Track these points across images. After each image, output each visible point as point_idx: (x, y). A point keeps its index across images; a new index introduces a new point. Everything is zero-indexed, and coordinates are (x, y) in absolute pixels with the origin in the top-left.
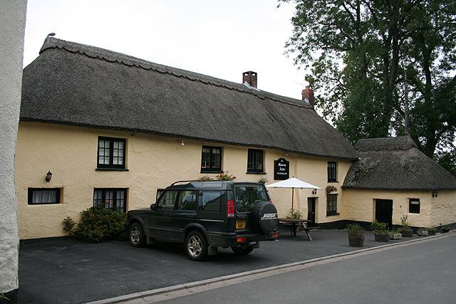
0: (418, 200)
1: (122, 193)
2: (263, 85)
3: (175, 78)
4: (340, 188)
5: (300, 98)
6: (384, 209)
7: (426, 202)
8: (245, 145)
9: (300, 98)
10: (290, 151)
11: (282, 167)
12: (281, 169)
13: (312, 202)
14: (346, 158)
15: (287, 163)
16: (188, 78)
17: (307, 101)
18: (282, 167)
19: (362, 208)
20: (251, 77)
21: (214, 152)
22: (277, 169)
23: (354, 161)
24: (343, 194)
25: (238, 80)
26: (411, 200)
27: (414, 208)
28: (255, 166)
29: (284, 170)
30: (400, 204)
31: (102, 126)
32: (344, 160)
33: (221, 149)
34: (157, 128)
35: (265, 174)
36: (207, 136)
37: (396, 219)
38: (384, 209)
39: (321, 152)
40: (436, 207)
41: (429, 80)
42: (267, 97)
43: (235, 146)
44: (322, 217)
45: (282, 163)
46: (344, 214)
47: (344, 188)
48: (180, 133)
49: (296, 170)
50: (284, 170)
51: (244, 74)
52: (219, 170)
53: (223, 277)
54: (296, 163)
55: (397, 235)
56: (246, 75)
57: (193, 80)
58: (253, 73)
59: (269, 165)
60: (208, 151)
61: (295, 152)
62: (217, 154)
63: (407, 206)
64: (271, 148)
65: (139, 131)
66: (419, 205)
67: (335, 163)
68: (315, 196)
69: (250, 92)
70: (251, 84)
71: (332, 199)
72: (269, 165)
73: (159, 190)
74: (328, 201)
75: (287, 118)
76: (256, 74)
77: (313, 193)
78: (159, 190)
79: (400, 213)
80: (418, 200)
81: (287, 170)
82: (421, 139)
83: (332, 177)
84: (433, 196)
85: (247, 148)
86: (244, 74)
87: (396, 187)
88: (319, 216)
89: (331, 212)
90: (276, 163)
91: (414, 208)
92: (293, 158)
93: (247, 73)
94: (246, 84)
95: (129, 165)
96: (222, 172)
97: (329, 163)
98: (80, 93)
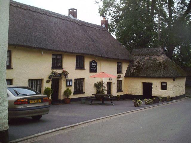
0: (166, 83)
1: (36, 81)
2: (81, 17)
3: (32, 12)
4: (123, 77)
5: (100, 24)
6: (147, 88)
7: (170, 84)
8: (75, 53)
9: (100, 24)
11: (94, 65)
12: (93, 67)
13: (109, 84)
14: (127, 60)
15: (96, 63)
16: (40, 13)
17: (104, 26)
18: (94, 65)
19: (136, 87)
20: (73, 12)
21: (58, 57)
22: (91, 66)
23: (131, 62)
24: (125, 81)
25: (66, 14)
26: (162, 83)
27: (164, 87)
28: (80, 66)
30: (156, 85)
31: (54, 50)
32: (126, 61)
33: (61, 55)
34: (29, 44)
35: (12, 69)
36: (56, 48)
38: (147, 88)
39: (114, 57)
40: (175, 86)
41: (170, 13)
42: (83, 25)
43: (70, 54)
44: (114, 93)
45: (93, 63)
46: (126, 90)
47: (125, 76)
48: (41, 46)
49: (101, 66)
50: (94, 67)
51: (69, 10)
52: (61, 68)
53: (85, 122)
54: (101, 64)
56: (70, 10)
57: (49, 16)
58: (75, 9)
59: (87, 65)
60: (55, 57)
63: (160, 86)
64: (88, 54)
65: (19, 45)
68: (111, 81)
71: (119, 83)
72: (87, 65)
73: (30, 80)
74: (118, 84)
76: (76, 10)
77: (110, 80)
78: (30, 80)
79: (157, 91)
80: (166, 83)
81: (96, 67)
82: (165, 48)
83: (119, 71)
84: (174, 80)
85: (76, 55)
86: (69, 10)
87: (168, 75)
88: (141, 90)
89: (119, 90)
90: (91, 63)
91: (164, 87)
92: (99, 60)
93: (71, 9)
94: (71, 16)
96: (63, 69)
97: (118, 62)
98: (33, 33)
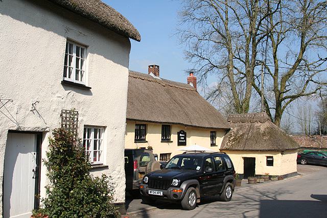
0: (272, 157)
2: (163, 75)
7: (277, 158)
10: (188, 125)
11: (182, 137)
15: (185, 134)
18: (182, 137)
20: (155, 69)
26: (268, 157)
27: (270, 163)
29: (183, 138)
30: (260, 160)
33: (145, 125)
37: (258, 171)
45: (182, 134)
50: (183, 138)
51: (150, 66)
55: (262, 180)
61: (191, 126)
62: (143, 130)
66: (273, 161)
67: (215, 132)
69: (156, 81)
70: (155, 74)
75: (183, 101)
79: (261, 167)
80: (272, 157)
86: (158, 67)
87: (269, 148)
89: (95, 160)
91: (270, 163)
93: (152, 66)
94: (152, 74)
95: (266, 158)
